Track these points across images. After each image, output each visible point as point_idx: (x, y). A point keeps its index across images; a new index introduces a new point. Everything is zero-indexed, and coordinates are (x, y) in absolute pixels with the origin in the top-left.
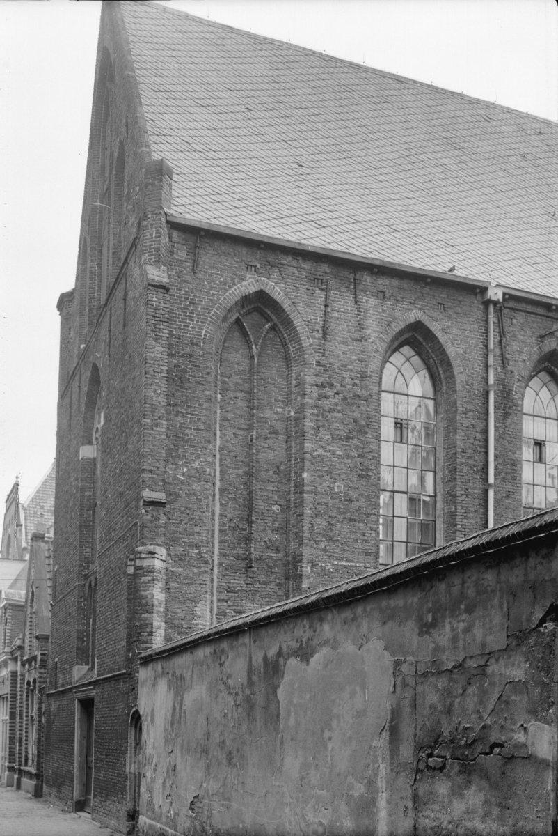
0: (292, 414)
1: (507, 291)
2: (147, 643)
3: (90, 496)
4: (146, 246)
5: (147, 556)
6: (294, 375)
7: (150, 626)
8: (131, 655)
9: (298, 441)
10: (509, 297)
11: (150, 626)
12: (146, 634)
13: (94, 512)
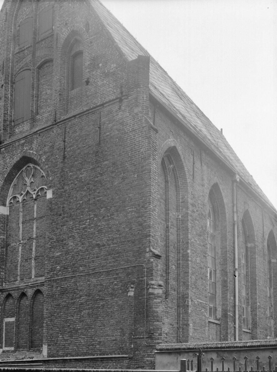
0: (180, 217)
2: (158, 339)
3: (4, 239)
4: (140, 103)
5: (158, 287)
6: (181, 197)
7: (160, 330)
8: (132, 346)
9: (184, 232)
11: (160, 330)
12: (157, 334)
13: (7, 250)
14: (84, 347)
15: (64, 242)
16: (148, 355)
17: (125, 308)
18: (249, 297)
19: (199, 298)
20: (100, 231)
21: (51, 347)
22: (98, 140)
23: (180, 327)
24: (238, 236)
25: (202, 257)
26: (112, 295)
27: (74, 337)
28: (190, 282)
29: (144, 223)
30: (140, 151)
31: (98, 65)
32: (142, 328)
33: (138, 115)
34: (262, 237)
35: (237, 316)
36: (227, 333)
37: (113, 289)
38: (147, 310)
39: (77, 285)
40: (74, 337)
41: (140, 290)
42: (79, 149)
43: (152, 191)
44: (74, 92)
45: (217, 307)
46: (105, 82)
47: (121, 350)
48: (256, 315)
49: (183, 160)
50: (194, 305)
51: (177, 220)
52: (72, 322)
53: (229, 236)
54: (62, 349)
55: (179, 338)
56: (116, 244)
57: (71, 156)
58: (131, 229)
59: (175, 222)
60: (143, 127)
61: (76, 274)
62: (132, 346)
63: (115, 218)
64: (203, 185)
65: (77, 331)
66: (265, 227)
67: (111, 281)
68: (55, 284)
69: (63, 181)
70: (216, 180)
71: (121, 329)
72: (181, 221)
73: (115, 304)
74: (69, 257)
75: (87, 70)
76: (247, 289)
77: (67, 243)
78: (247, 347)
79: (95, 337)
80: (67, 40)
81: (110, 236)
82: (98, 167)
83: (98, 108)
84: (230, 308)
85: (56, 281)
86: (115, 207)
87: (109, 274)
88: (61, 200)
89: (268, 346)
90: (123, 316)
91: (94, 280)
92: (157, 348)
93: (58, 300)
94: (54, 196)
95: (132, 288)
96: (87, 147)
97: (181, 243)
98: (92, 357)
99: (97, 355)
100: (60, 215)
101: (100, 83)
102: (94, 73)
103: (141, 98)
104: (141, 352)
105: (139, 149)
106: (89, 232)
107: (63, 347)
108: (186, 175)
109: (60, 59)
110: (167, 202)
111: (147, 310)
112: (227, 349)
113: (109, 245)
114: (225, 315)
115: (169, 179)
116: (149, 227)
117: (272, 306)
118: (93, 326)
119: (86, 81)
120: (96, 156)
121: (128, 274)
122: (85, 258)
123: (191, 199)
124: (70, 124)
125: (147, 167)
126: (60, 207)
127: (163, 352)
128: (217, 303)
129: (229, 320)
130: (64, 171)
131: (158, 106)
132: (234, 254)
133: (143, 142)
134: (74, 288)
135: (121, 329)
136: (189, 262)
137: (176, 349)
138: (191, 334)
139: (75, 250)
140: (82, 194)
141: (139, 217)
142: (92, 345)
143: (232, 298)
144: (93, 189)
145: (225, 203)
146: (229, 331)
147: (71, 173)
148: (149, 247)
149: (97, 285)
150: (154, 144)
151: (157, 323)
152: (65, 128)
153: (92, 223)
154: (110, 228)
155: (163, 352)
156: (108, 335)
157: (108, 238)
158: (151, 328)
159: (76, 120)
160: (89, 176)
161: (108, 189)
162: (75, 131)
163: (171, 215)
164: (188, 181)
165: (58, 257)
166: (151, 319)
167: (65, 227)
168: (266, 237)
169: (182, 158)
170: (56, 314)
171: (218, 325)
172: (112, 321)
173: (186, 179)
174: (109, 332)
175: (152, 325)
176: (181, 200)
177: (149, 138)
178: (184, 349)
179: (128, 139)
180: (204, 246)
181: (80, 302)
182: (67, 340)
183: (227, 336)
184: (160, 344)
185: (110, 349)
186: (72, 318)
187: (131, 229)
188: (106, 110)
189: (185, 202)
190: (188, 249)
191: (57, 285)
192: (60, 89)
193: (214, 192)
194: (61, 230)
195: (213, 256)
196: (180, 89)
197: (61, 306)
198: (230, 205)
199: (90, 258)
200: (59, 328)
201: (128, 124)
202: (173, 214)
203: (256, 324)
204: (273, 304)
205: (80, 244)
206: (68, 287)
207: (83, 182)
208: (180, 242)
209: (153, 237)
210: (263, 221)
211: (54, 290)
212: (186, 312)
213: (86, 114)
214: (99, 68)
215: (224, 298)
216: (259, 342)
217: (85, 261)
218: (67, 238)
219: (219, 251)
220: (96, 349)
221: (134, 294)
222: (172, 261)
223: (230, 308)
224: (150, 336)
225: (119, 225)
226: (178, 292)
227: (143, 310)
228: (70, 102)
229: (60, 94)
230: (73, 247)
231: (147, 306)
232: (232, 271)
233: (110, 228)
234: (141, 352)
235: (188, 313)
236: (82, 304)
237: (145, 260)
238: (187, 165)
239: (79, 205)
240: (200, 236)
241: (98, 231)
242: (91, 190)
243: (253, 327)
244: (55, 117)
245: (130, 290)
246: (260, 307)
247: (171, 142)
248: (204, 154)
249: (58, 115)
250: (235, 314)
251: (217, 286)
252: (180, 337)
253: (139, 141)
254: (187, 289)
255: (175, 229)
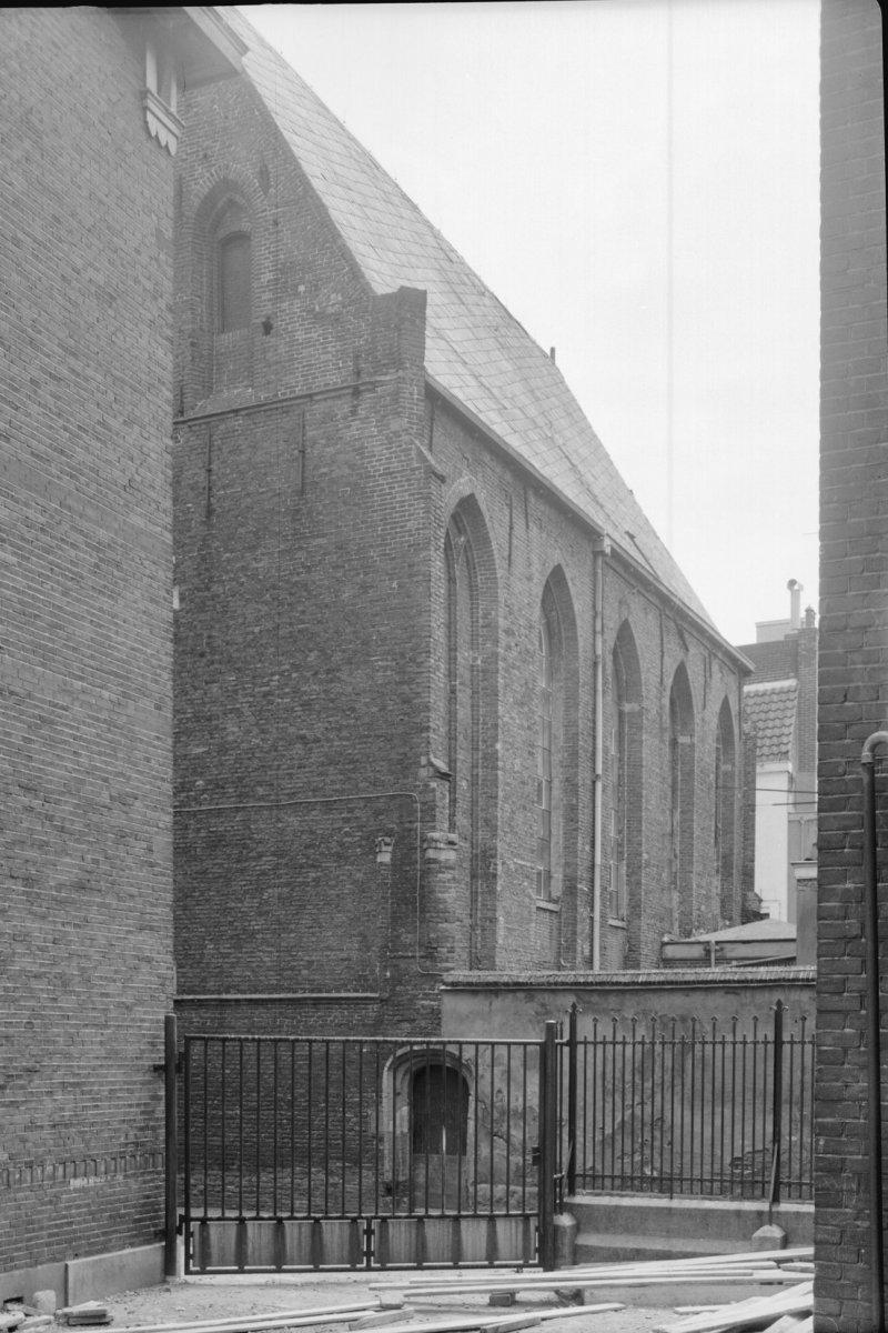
0: (479, 662)
1: (615, 547)
2: (447, 961)
4: (404, 408)
8: (388, 974)
10: (614, 553)
14: (271, 973)
15: (214, 723)
16: (425, 994)
17: (370, 888)
18: (622, 840)
19: (518, 856)
20: (306, 705)
21: (184, 970)
22: (299, 482)
23: (477, 925)
24: (603, 690)
25: (526, 755)
26: (339, 856)
27: (244, 950)
28: (500, 819)
29: (414, 698)
30: (405, 526)
31: (296, 286)
32: (409, 936)
33: (400, 436)
34: (658, 685)
35: (597, 892)
36: (574, 933)
37: (341, 844)
38: (423, 897)
39: (249, 828)
40: (244, 950)
41: (405, 851)
42: (248, 495)
43: (432, 624)
44: (227, 339)
45: (553, 870)
46: (315, 335)
47: (363, 982)
48: (639, 883)
49: (489, 525)
50: (508, 873)
51: (473, 671)
52: (240, 915)
53: (584, 696)
54: (217, 976)
55: (474, 950)
56: (348, 739)
57: (229, 510)
58: (383, 708)
59: (467, 675)
60: (413, 470)
61: (247, 802)
62: (388, 974)
63: (344, 677)
64: (529, 579)
65: (253, 934)
66: (666, 658)
67: (336, 826)
68: (192, 822)
69: (207, 570)
70: (556, 557)
71: (360, 934)
72: (483, 671)
73: (345, 878)
74: (229, 759)
75: (266, 296)
76: (619, 821)
77: (223, 726)
78: (637, 983)
79: (298, 951)
80: (210, 200)
81: (331, 719)
82: (301, 548)
83: (298, 401)
84: (582, 872)
85: (195, 816)
86: (344, 652)
87: (331, 810)
88: (202, 617)
89: (681, 983)
90: (365, 907)
91: (293, 821)
92: (446, 980)
93: (202, 861)
94: (184, 606)
95: (387, 844)
96: (270, 494)
97: (481, 726)
98: (290, 995)
99: (304, 991)
100: (202, 655)
101: (300, 336)
102: (285, 305)
103: (407, 395)
104: (409, 988)
105: (402, 521)
106: (278, 704)
107: (217, 970)
108: (493, 560)
109: (190, 249)
110: (453, 629)
111: (423, 897)
112: (599, 988)
113: (328, 740)
114: (571, 890)
115: (457, 573)
116: (427, 709)
117: (675, 856)
118: (293, 926)
119: (263, 323)
120: (294, 520)
121: (377, 813)
122: (270, 767)
123: (505, 618)
124: (222, 427)
125: (423, 569)
126: (201, 635)
127: (458, 989)
128: (553, 864)
129: (579, 903)
130: (209, 546)
131: (439, 403)
132: (594, 738)
133: (413, 505)
134: (243, 835)
135: (360, 934)
136: (500, 772)
137: (488, 984)
138: (500, 942)
139: (245, 745)
140: (260, 611)
141: (401, 683)
142: (292, 969)
143: (587, 848)
144: (289, 601)
145: (576, 613)
146: (579, 927)
147: (227, 555)
148: (427, 754)
149: (302, 832)
150: (438, 511)
151: (445, 925)
152: (211, 436)
153: (287, 684)
154: (332, 701)
155: (458, 989)
156: (329, 948)
157: (327, 725)
158: (432, 935)
159: (238, 422)
160: (278, 569)
161: (326, 606)
162: (236, 451)
163: (460, 659)
164: (499, 576)
165: (197, 757)
166: (432, 917)
167: (215, 688)
168: (669, 681)
169: (487, 520)
170: (197, 894)
171: (554, 915)
172: (340, 918)
173: (495, 569)
174: (333, 942)
175: (435, 931)
176: (481, 621)
177: (428, 498)
178: (506, 984)
179: (375, 491)
180: (529, 728)
181: (258, 868)
182: (227, 956)
183: (575, 941)
184: (452, 972)
185: (335, 980)
186: (239, 905)
187: (383, 708)
188: (320, 408)
189: (491, 626)
190: (497, 741)
191: (199, 826)
192: (194, 330)
193: (556, 583)
194: (206, 694)
195: (546, 746)
196: (452, 255)
197: (210, 876)
198: (588, 616)
199: (283, 767)
200: (206, 927)
201: (375, 456)
202: (464, 655)
203: (639, 906)
204: (678, 852)
205: (255, 731)
206: (226, 831)
207: (260, 580)
208: (478, 724)
209: (434, 730)
210: (662, 644)
211: (191, 836)
212: (492, 892)
213: (265, 411)
214: (297, 294)
215: (570, 848)
216: (662, 974)
217: (269, 773)
218: (220, 714)
219: (560, 733)
220: (300, 978)
221: (392, 859)
222: (461, 769)
223: (582, 872)
224: (430, 952)
225: (354, 697)
226: (472, 842)
227: (410, 893)
228: (218, 364)
229: (193, 344)
230: (238, 737)
231: (422, 887)
232: (589, 782)
233: (332, 701)
234: (409, 988)
235: (494, 893)
236: (264, 873)
237: (418, 783)
238: (497, 534)
239: (251, 637)
240: (522, 704)
241: (301, 705)
242: (282, 604)
243: (632, 913)
244: (182, 402)
245: (384, 848)
246: (857, 1284)
247: (463, 484)
248: (532, 499)
249: (189, 399)
250: (593, 886)
251: (554, 819)
252: (476, 948)
253: (403, 501)
254: (494, 836)
255: (469, 691)
